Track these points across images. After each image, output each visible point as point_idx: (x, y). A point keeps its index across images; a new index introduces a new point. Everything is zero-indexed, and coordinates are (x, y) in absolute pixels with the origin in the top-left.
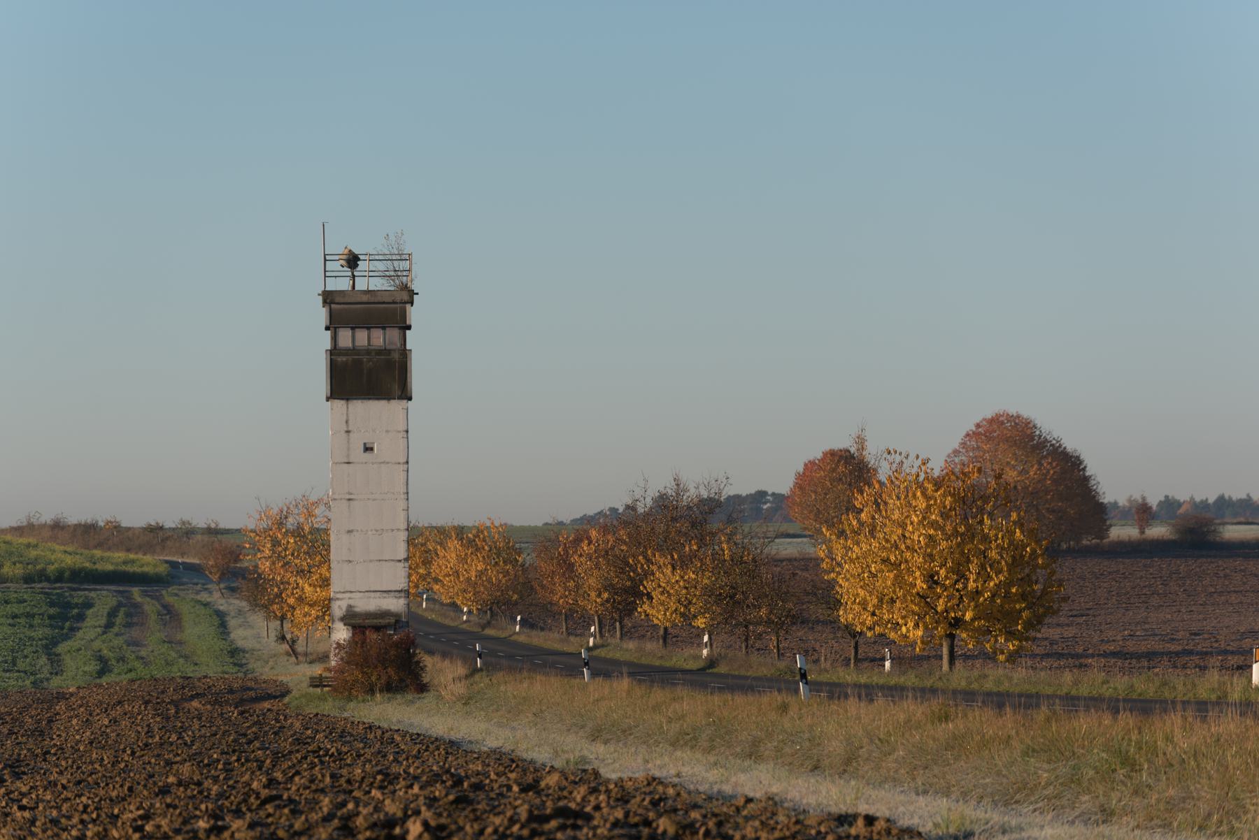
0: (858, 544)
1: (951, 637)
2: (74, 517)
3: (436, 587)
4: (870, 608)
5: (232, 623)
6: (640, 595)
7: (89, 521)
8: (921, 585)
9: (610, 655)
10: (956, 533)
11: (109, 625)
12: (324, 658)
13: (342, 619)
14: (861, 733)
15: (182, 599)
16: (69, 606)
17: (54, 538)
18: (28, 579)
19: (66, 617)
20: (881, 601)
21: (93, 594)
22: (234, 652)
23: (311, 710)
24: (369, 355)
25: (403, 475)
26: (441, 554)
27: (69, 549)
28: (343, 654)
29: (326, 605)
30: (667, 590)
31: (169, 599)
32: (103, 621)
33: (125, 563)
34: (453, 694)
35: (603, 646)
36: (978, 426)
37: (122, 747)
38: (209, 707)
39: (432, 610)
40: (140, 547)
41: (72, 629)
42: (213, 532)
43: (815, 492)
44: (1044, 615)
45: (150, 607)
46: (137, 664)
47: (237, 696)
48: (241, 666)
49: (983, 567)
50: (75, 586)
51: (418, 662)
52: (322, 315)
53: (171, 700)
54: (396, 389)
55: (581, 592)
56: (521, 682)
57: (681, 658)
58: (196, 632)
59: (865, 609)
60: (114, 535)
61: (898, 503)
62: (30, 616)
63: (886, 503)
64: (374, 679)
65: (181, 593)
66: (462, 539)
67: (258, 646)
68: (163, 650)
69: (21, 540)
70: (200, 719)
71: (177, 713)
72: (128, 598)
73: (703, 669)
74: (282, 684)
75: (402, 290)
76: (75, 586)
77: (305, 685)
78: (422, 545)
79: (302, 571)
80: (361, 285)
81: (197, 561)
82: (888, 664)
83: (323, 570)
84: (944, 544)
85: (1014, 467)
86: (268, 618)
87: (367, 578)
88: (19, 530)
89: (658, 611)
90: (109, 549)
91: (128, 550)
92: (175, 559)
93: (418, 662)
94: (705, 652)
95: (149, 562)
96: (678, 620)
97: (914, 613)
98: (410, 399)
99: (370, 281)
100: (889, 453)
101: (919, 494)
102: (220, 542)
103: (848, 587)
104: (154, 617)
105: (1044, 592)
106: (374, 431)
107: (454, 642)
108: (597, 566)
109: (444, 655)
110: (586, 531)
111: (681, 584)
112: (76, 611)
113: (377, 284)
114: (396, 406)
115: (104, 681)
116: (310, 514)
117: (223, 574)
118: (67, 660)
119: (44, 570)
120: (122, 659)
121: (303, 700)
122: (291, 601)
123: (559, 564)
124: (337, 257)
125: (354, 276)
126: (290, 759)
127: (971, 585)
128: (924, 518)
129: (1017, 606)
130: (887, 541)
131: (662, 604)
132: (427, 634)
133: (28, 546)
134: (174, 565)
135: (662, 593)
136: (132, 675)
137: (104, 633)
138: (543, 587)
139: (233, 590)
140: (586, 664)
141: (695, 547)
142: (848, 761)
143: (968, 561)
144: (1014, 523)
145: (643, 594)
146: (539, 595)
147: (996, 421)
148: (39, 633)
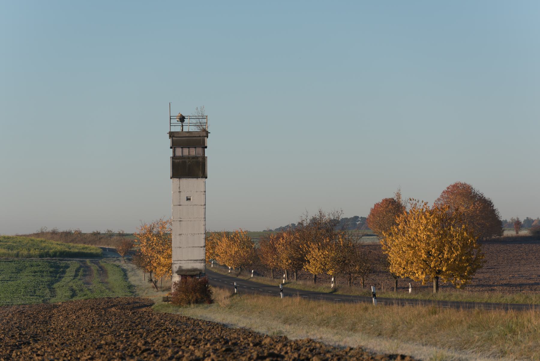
0: (397, 239)
1: (437, 278)
3: (217, 258)
4: (403, 266)
5: (129, 274)
6: (304, 261)
7: (68, 231)
8: (424, 256)
9: (292, 287)
10: (439, 234)
11: (76, 276)
12: (169, 289)
13: (177, 272)
15: (107, 264)
16: (58, 267)
17: (52, 238)
18: (41, 256)
19: (57, 272)
21: (69, 262)
22: (130, 287)
23: (163, 311)
24: (189, 159)
25: (203, 210)
27: (59, 243)
28: (177, 287)
29: (170, 266)
30: (316, 259)
31: (102, 264)
32: (73, 274)
33: (83, 248)
34: (224, 304)
35: (289, 283)
36: (448, 188)
37: (81, 328)
38: (119, 310)
39: (215, 268)
41: (60, 277)
43: (379, 217)
45: (94, 267)
46: (88, 292)
47: (131, 306)
48: (133, 292)
49: (450, 248)
52: (168, 142)
53: (103, 307)
54: (201, 174)
55: (279, 260)
56: (253, 299)
57: (322, 288)
58: (114, 278)
60: (79, 237)
63: (409, 221)
64: (190, 298)
67: (140, 284)
68: (100, 286)
69: (38, 239)
70: (115, 316)
71: (105, 313)
72: (84, 264)
73: (331, 293)
78: (211, 240)
79: (160, 252)
80: (186, 129)
82: (410, 290)
83: (169, 251)
85: (463, 205)
86: (145, 272)
87: (188, 254)
88: (37, 235)
89: (312, 268)
90: (76, 243)
91: (85, 243)
92: (105, 247)
94: (332, 285)
95: (94, 248)
96: (321, 271)
97: (421, 268)
99: (190, 127)
100: (411, 200)
101: (423, 217)
103: (393, 257)
104: (95, 272)
107: (225, 282)
109: (221, 287)
110: (282, 234)
111: (322, 256)
112: (62, 269)
113: (193, 129)
114: (200, 181)
115: (74, 299)
118: (58, 291)
119: (48, 252)
120: (81, 290)
122: (155, 265)
123: (270, 248)
125: (183, 126)
127: (445, 256)
128: (426, 227)
131: (314, 265)
133: (41, 241)
134: (104, 249)
135: (314, 260)
136: (86, 297)
137: (74, 279)
138: (263, 258)
140: (282, 291)
141: (328, 240)
142: (394, 332)
143: (444, 246)
144: (463, 229)
145: (306, 261)
146: (263, 261)
147: (455, 186)
148: (46, 279)
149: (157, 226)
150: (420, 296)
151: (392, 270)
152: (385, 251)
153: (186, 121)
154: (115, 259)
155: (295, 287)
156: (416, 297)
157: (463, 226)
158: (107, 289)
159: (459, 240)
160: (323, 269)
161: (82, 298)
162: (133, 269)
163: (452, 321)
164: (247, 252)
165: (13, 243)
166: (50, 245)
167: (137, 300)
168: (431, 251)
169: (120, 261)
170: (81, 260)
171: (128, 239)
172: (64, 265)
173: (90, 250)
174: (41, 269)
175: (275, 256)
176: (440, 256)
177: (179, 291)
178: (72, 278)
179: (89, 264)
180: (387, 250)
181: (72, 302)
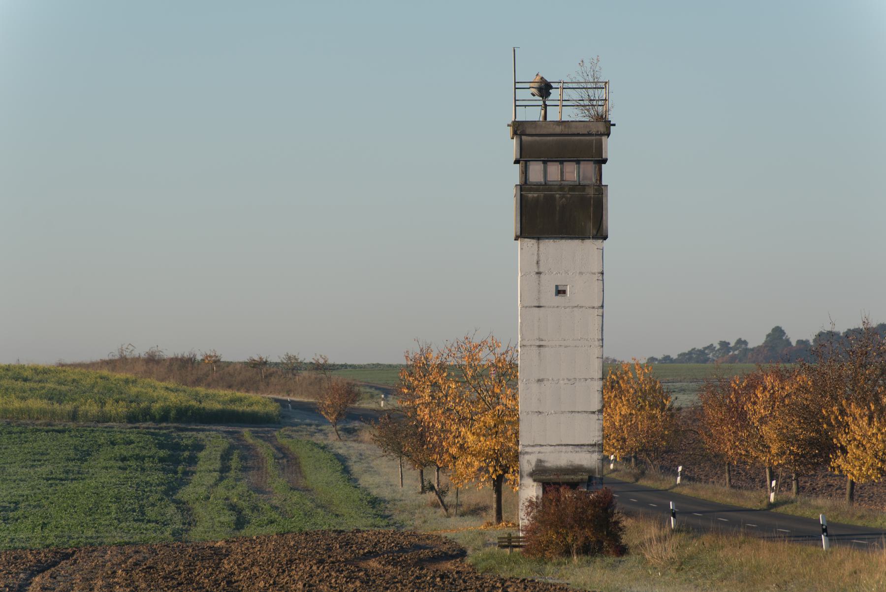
2: (170, 350)
6: (833, 448)
7: (186, 355)
9: (799, 513)
11: (225, 469)
13: (531, 475)
15: (296, 439)
16: (176, 447)
17: (148, 373)
18: (132, 418)
19: (178, 461)
21: (201, 435)
22: (375, 502)
24: (562, 190)
25: (598, 320)
27: (171, 385)
31: (284, 442)
32: (218, 465)
33: (232, 401)
41: (185, 473)
45: (264, 449)
46: (274, 515)
48: (384, 517)
50: (183, 426)
51: (617, 523)
52: (512, 147)
54: (591, 228)
58: (320, 477)
60: (214, 370)
62: (140, 458)
64: (569, 539)
65: (294, 435)
68: (295, 499)
69: (118, 376)
72: (238, 439)
76: (183, 426)
79: (465, 419)
80: (553, 115)
82: (679, 478)
88: (110, 364)
91: (230, 387)
93: (617, 523)
95: (259, 401)
99: (564, 111)
106: (566, 272)
111: (880, 437)
113: (572, 114)
114: (591, 245)
115: (246, 532)
116: (472, 357)
117: (340, 414)
119: (149, 408)
120: (255, 508)
122: (454, 450)
124: (528, 85)
125: (546, 106)
131: (858, 459)
133: (127, 381)
134: (283, 403)
137: (221, 479)
140: (825, 531)
145: (837, 448)
153: (554, 94)
154: (313, 428)
158: (318, 506)
165: (60, 384)
166: (150, 390)
169: (325, 434)
172: (190, 442)
173: (251, 404)
174: (137, 451)
179: (251, 441)
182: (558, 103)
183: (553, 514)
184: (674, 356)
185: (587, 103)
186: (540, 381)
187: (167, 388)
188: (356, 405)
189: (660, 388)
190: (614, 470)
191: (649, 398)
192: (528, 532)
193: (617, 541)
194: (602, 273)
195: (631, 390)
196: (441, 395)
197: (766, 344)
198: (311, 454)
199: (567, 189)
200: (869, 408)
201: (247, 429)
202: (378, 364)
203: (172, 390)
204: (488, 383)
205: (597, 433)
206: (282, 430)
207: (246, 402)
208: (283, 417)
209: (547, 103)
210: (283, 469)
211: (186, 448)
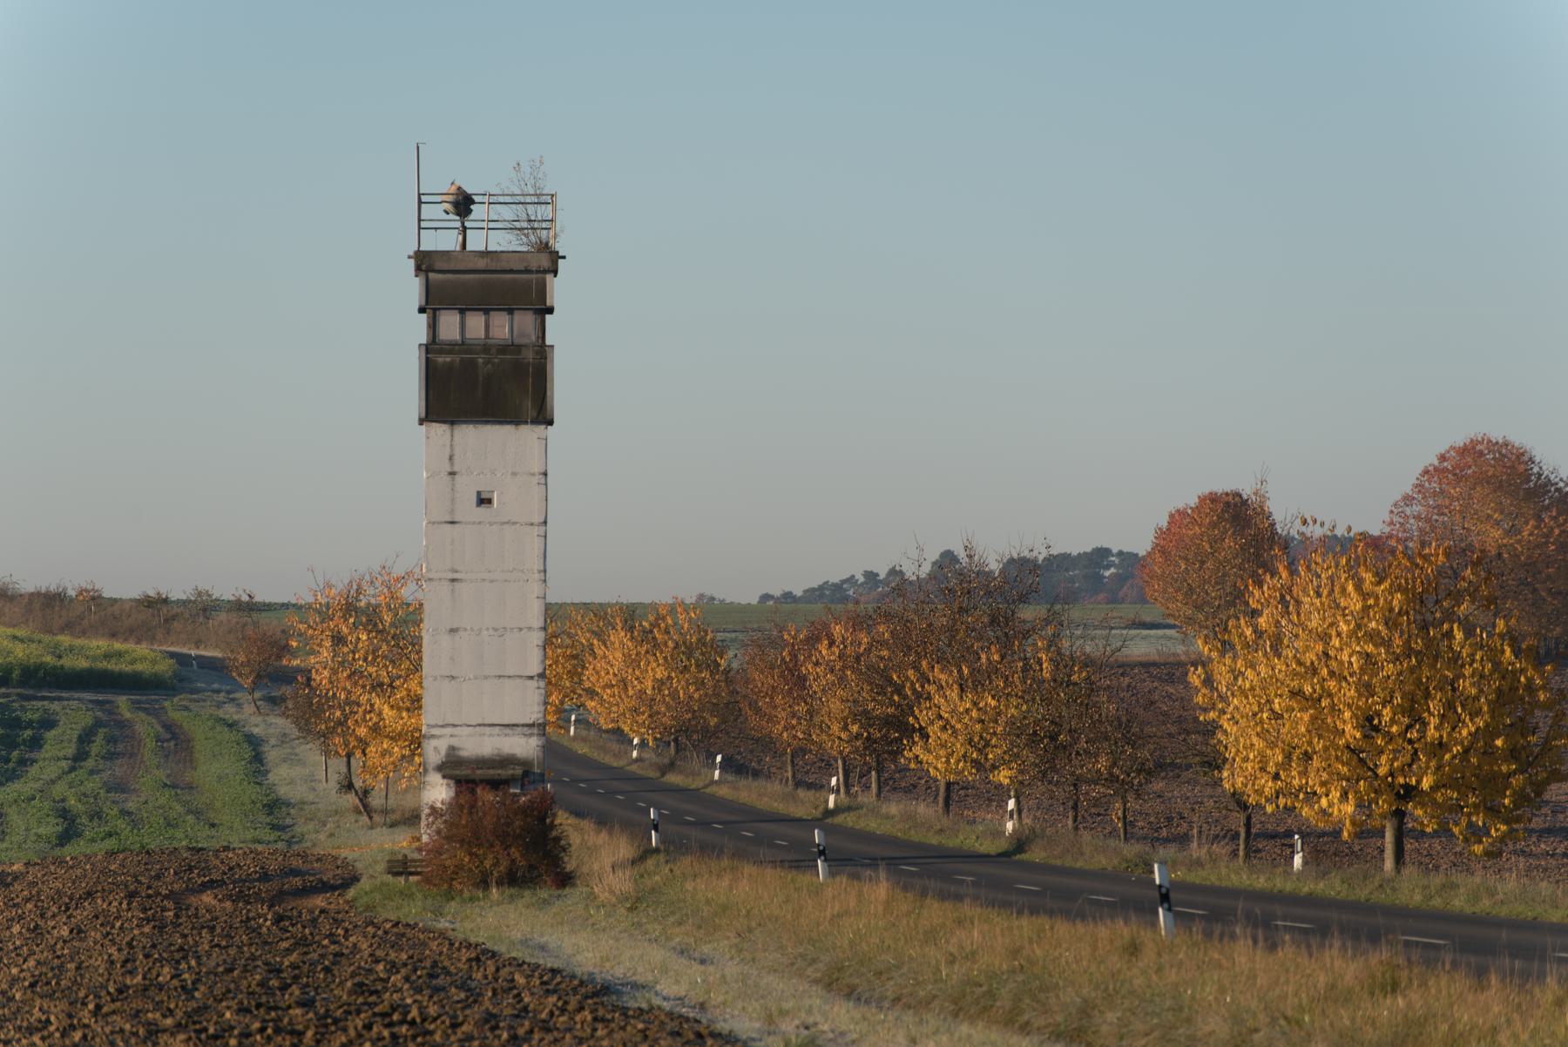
0: (1253, 667)
1: (1399, 815)
3: (591, 704)
4: (1271, 768)
5: (272, 754)
6: (908, 731)
7: (53, 588)
8: (1352, 733)
9: (861, 825)
10: (1408, 652)
11: (80, 756)
12: (412, 819)
14: (1254, 1004)
15: (192, 714)
16: (16, 724)
20: (1288, 757)
21: (56, 706)
22: (274, 805)
23: (388, 913)
24: (488, 355)
25: (539, 542)
26: (599, 652)
27: (20, 633)
28: (440, 824)
29: (415, 741)
30: (952, 725)
31: (175, 715)
32: (71, 751)
33: (107, 656)
34: (612, 892)
35: (849, 809)
36: (1443, 458)
37: (82, 994)
38: (228, 904)
39: (584, 740)
40: (131, 631)
41: (23, 762)
42: (247, 607)
43: (1186, 559)
44: (1547, 782)
45: (146, 728)
46: (121, 824)
47: (274, 886)
48: (283, 828)
49: (1450, 706)
50: (31, 692)
52: (412, 289)
53: (167, 890)
55: (817, 719)
56: (719, 876)
58: (216, 769)
59: (1263, 769)
61: (1317, 601)
63: (1298, 603)
64: (488, 864)
65: (192, 705)
66: (631, 629)
67: (311, 797)
68: (162, 801)
70: (212, 929)
71: (177, 916)
72: (111, 713)
73: (1005, 854)
74: (346, 864)
75: (539, 251)
76: (31, 692)
77: (381, 867)
78: (571, 634)
79: (381, 685)
80: (476, 242)
81: (219, 655)
82: (1298, 860)
83: (413, 685)
84: (1390, 669)
85: (1498, 523)
86: (327, 753)
87: (480, 700)
89: (937, 758)
90: (84, 633)
91: (113, 635)
92: (185, 651)
94: (1010, 826)
95: (144, 656)
96: (970, 775)
97: (1341, 777)
98: (551, 423)
99: (491, 236)
100: (1305, 522)
101: (1350, 588)
102: (256, 624)
104: (150, 744)
105: (1546, 745)
107: (617, 798)
108: (842, 679)
109: (602, 822)
110: (826, 626)
112: (28, 733)
113: (502, 242)
115: (68, 851)
117: (259, 677)
120: (97, 815)
121: (378, 896)
122: (362, 731)
123: (782, 675)
124: (438, 198)
125: (465, 229)
126: (345, 1030)
127: (1431, 733)
128: (1359, 626)
129: (1504, 768)
130: (1300, 663)
131: (943, 746)
132: (575, 781)
134: (183, 660)
135: (944, 728)
136: (111, 844)
137: (72, 769)
138: (758, 710)
139: (273, 701)
141: (996, 657)
143: (1427, 695)
144: (1502, 636)
145: (914, 730)
147: (1471, 451)
149: (371, 591)
150: (1332, 886)
151: (1232, 779)
152: (1205, 710)
153: (478, 211)
155: (873, 825)
156: (1321, 887)
157: (1501, 625)
158: (190, 812)
159: (1482, 676)
160: (975, 762)
161: (96, 847)
162: (284, 738)
163: (1460, 1027)
164: (701, 684)
167: (297, 863)
168: (1379, 714)
169: (239, 705)
170: (101, 697)
171: (268, 623)
172: (36, 716)
175: (801, 708)
176: (1413, 735)
177: (448, 838)
178: (65, 764)
179: (128, 715)
180: (1214, 708)
181: (60, 862)
182: (484, 225)
183: (465, 826)
184: (798, 593)
185: (525, 225)
186: (453, 631)
187: (15, 637)
188: (284, 662)
189: (712, 640)
190: (637, 760)
191: (697, 654)
192: (428, 852)
193: (557, 866)
194: (545, 474)
195: (670, 643)
196: (345, 650)
197: (932, 577)
198: (210, 734)
199: (493, 351)
200: (960, 671)
201: (125, 698)
202: (956, 582)
203: (22, 641)
204: (386, 632)
205: (536, 708)
206: (176, 700)
207: (128, 658)
208: (181, 680)
209: (467, 224)
210: (167, 756)
211: (30, 724)
